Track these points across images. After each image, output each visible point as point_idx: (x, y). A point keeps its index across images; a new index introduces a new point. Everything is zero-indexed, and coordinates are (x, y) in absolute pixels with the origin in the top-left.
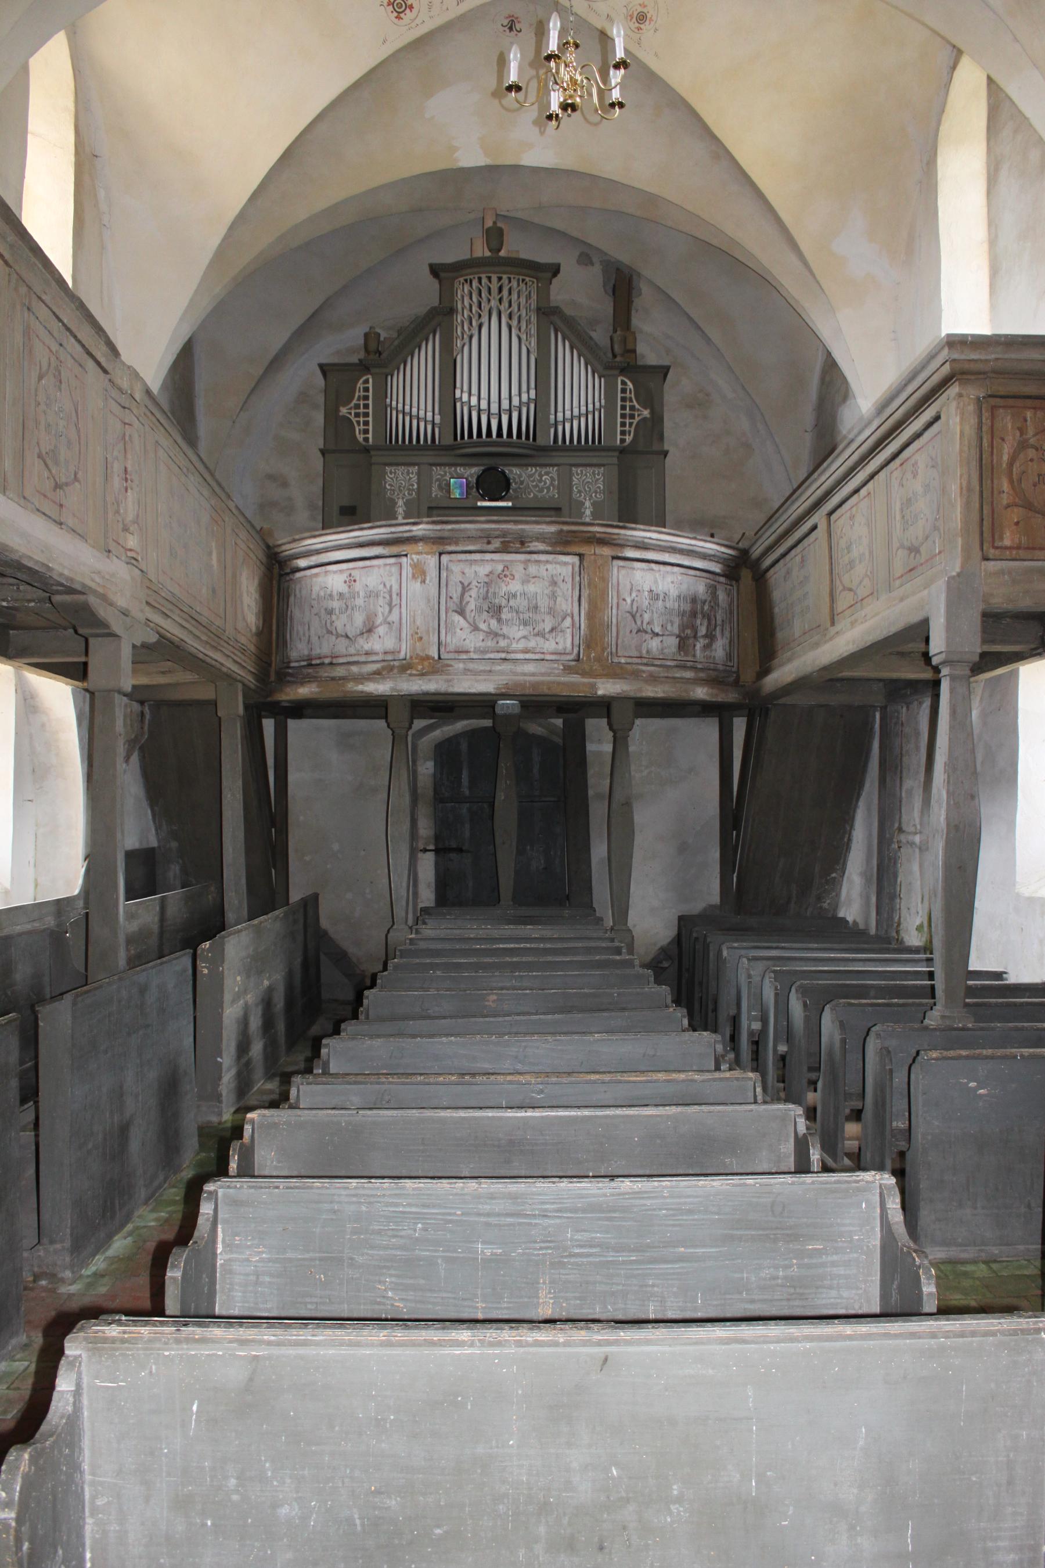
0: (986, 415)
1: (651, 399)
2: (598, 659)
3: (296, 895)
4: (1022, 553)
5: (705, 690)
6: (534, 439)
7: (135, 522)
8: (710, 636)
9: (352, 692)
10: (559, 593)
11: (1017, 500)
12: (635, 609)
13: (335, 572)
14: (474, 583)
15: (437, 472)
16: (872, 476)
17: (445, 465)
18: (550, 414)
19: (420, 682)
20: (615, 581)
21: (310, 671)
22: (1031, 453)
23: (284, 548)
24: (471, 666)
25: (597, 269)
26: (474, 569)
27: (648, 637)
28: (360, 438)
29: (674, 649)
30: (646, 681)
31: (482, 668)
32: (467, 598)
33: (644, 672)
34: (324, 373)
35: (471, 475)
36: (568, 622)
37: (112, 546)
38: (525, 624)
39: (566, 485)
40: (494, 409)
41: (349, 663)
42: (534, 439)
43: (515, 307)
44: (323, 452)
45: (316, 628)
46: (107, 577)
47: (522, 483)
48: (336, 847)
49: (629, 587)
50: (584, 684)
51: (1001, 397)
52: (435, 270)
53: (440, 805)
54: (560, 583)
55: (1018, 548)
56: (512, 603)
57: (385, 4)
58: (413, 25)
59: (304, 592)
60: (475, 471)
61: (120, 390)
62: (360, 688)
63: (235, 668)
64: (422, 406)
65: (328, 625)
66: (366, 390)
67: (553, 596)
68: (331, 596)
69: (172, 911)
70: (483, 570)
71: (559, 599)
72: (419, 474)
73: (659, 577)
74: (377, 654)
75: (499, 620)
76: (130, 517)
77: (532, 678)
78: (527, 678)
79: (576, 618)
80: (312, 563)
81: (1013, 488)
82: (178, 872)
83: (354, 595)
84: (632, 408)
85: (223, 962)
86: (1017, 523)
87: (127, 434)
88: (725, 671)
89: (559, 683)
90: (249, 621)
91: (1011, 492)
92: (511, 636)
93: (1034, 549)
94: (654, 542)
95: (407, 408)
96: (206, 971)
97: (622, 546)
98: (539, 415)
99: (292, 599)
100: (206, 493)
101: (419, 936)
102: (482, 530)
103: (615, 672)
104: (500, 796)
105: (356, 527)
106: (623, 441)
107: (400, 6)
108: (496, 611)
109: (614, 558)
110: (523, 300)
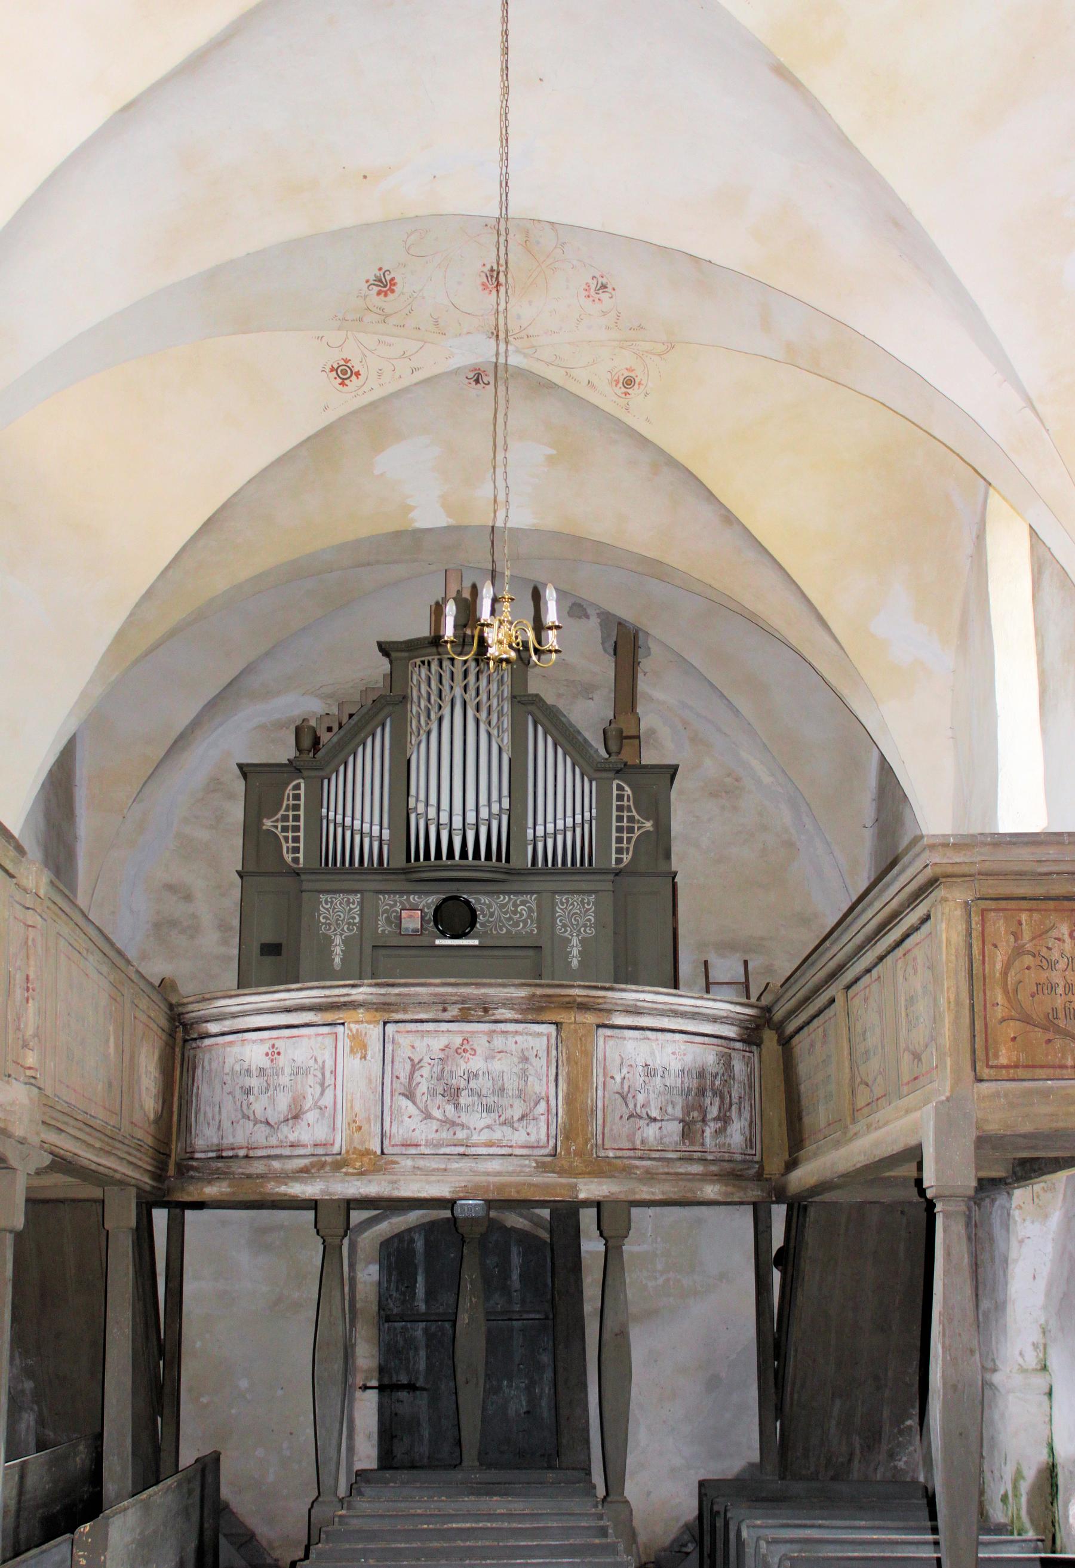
0: (976, 919)
2: (579, 1154)
3: (187, 1457)
4: (1021, 1073)
5: (717, 1188)
6: (508, 860)
7: (36, 1035)
8: (724, 1119)
9: (273, 1194)
10: (531, 1071)
11: (1013, 1013)
12: (626, 1089)
13: (254, 1041)
14: (427, 1060)
15: (385, 901)
16: (881, 958)
17: (395, 892)
18: (526, 828)
19: (358, 1183)
20: (601, 1055)
21: (220, 1165)
22: (1028, 960)
23: (190, 1007)
24: (421, 1163)
25: (594, 622)
26: (425, 1043)
27: (642, 1123)
28: (288, 858)
29: (677, 1138)
30: (640, 1180)
31: (435, 1165)
32: (417, 1078)
33: (637, 1167)
34: (245, 775)
35: (428, 906)
36: (542, 1107)
37: (11, 1068)
38: (489, 1110)
39: (545, 917)
40: (457, 823)
41: (269, 1157)
42: (508, 860)
43: (484, 696)
44: (240, 874)
45: (229, 1110)
46: (8, 1108)
47: (492, 915)
48: (244, 1384)
49: (618, 1062)
50: (562, 1185)
51: (992, 899)
52: (385, 649)
53: (386, 1325)
54: (533, 1059)
55: (1016, 1066)
56: (472, 1084)
57: (328, 370)
58: (360, 392)
59: (214, 1065)
60: (433, 900)
61: (25, 890)
62: (283, 1189)
63: (130, 1172)
64: (367, 818)
65: (245, 1107)
66: (297, 797)
67: (524, 1075)
68: (248, 1071)
69: (31, 1481)
70: (437, 1044)
71: (530, 1079)
72: (361, 904)
73: (659, 1049)
74: (305, 1146)
75: (457, 1106)
76: (30, 1031)
77: (497, 1179)
78: (491, 1179)
79: (553, 1103)
81: (1009, 1001)
82: (32, 1423)
83: (277, 1072)
84: (631, 819)
85: (106, 1548)
86: (1014, 1039)
87: (30, 938)
88: (744, 1161)
89: (531, 1185)
90: (146, 1108)
91: (1006, 1004)
92: (472, 1127)
93: (1033, 1067)
95: (348, 820)
96: (83, 1562)
97: (610, 1011)
98: (513, 829)
99: (199, 1072)
100: (105, 969)
101: (351, 1513)
102: (436, 995)
103: (600, 1169)
104: (463, 1319)
105: (282, 987)
106: (619, 861)
107: (344, 372)
108: (453, 1094)
110: (494, 687)
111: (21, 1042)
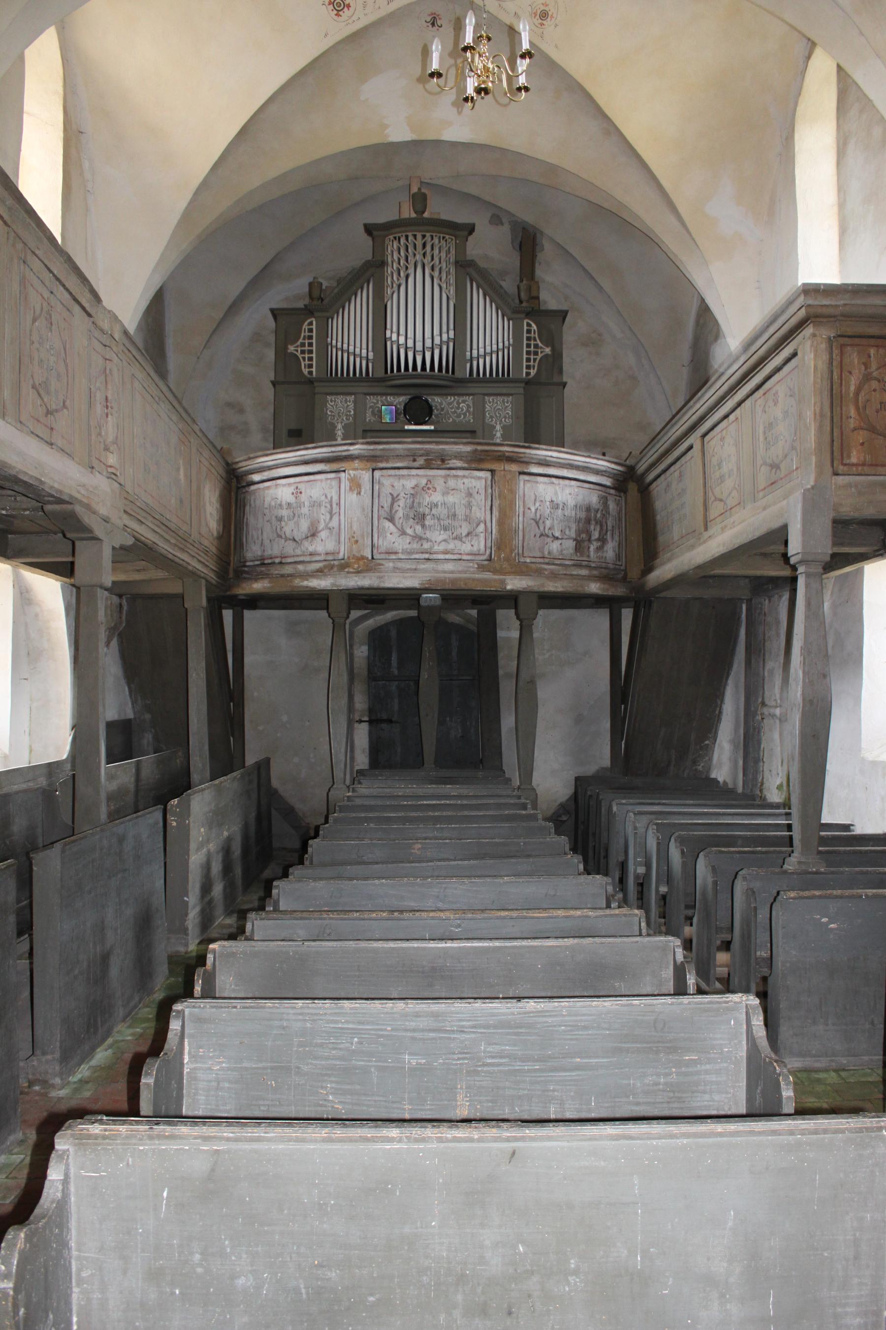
0: (836, 352)
1: (552, 338)
2: (507, 559)
3: (251, 760)
4: (866, 469)
5: (598, 585)
6: (453, 372)
7: (115, 442)
8: (602, 540)
9: (298, 587)
10: (474, 503)
11: (862, 424)
12: (538, 517)
13: (284, 485)
14: (402, 495)
15: (371, 400)
16: (739, 404)
17: (377, 394)
18: (466, 351)
19: (356, 579)
20: (521, 493)
21: (263, 569)
22: (874, 384)
23: (241, 465)
24: (399, 565)
25: (506, 228)
26: (402, 483)
27: (549, 540)
28: (305, 371)
29: (572, 551)
30: (548, 578)
31: (408, 567)
32: (396, 507)
33: (546, 570)
34: (275, 317)
35: (400, 403)
36: (481, 527)
37: (95, 463)
38: (445, 529)
39: (480, 411)
40: (419, 347)
41: (296, 562)
42: (453, 372)
43: (436, 260)
44: (274, 384)
45: (268, 532)
46: (91, 489)
47: (442, 409)
48: (285, 718)
49: (533, 498)
50: (495, 580)
51: (849, 337)
52: (369, 229)
53: (373, 683)
54: (475, 495)
55: (863, 465)
56: (434, 511)
57: (327, 3)
58: (350, 21)
59: (258, 502)
60: (403, 399)
61: (102, 330)
62: (305, 583)
63: (199, 567)
64: (358, 345)
65: (278, 530)
66: (311, 330)
67: (469, 506)
68: (280, 505)
69: (146, 772)
70: (410, 484)
71: (474, 508)
72: (355, 402)
73: (559, 490)
74: (319, 554)
75: (423, 526)
76: (110, 438)
77: (451, 575)
78: (447, 575)
79: (489, 524)
80: (265, 478)
81: (859, 414)
82: (151, 739)
83: (300, 505)
84: (536, 346)
85: (189, 816)
86: (862, 444)
87: (108, 368)
88: (615, 569)
89: (474, 580)
90: (211, 526)
91: (857, 417)
92: (433, 540)
93: (876, 465)
94: (555, 460)
95: (345, 346)
96: (174, 824)
97: (528, 463)
98: (457, 352)
99: (247, 508)
100: (174, 418)
101: (355, 794)
102: (409, 450)
103: (521, 570)
104: (424, 675)
105: (302, 447)
106: (528, 374)
107: (339, 5)
108: (421, 518)
109: (521, 473)
110: (443, 255)
111: (102, 446)
